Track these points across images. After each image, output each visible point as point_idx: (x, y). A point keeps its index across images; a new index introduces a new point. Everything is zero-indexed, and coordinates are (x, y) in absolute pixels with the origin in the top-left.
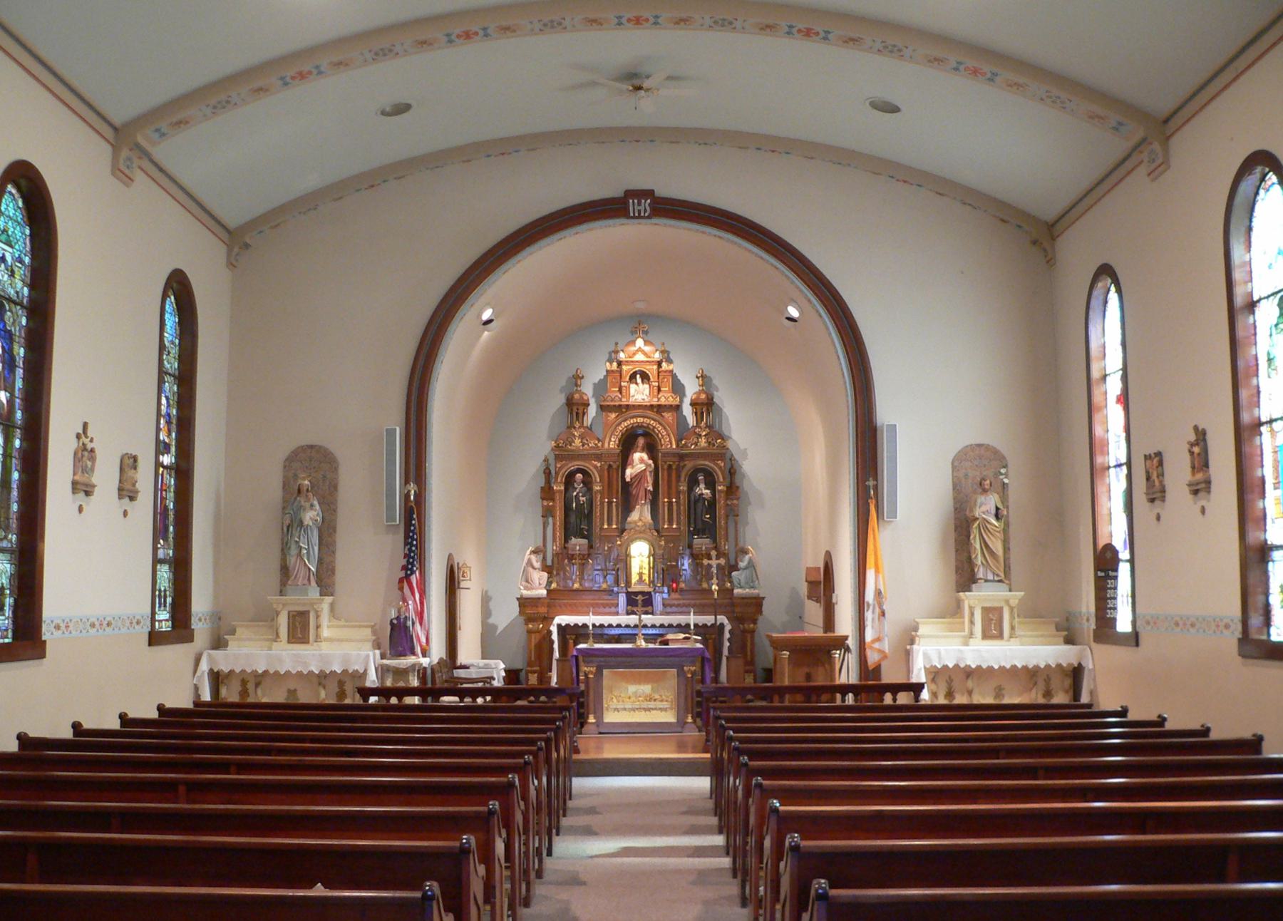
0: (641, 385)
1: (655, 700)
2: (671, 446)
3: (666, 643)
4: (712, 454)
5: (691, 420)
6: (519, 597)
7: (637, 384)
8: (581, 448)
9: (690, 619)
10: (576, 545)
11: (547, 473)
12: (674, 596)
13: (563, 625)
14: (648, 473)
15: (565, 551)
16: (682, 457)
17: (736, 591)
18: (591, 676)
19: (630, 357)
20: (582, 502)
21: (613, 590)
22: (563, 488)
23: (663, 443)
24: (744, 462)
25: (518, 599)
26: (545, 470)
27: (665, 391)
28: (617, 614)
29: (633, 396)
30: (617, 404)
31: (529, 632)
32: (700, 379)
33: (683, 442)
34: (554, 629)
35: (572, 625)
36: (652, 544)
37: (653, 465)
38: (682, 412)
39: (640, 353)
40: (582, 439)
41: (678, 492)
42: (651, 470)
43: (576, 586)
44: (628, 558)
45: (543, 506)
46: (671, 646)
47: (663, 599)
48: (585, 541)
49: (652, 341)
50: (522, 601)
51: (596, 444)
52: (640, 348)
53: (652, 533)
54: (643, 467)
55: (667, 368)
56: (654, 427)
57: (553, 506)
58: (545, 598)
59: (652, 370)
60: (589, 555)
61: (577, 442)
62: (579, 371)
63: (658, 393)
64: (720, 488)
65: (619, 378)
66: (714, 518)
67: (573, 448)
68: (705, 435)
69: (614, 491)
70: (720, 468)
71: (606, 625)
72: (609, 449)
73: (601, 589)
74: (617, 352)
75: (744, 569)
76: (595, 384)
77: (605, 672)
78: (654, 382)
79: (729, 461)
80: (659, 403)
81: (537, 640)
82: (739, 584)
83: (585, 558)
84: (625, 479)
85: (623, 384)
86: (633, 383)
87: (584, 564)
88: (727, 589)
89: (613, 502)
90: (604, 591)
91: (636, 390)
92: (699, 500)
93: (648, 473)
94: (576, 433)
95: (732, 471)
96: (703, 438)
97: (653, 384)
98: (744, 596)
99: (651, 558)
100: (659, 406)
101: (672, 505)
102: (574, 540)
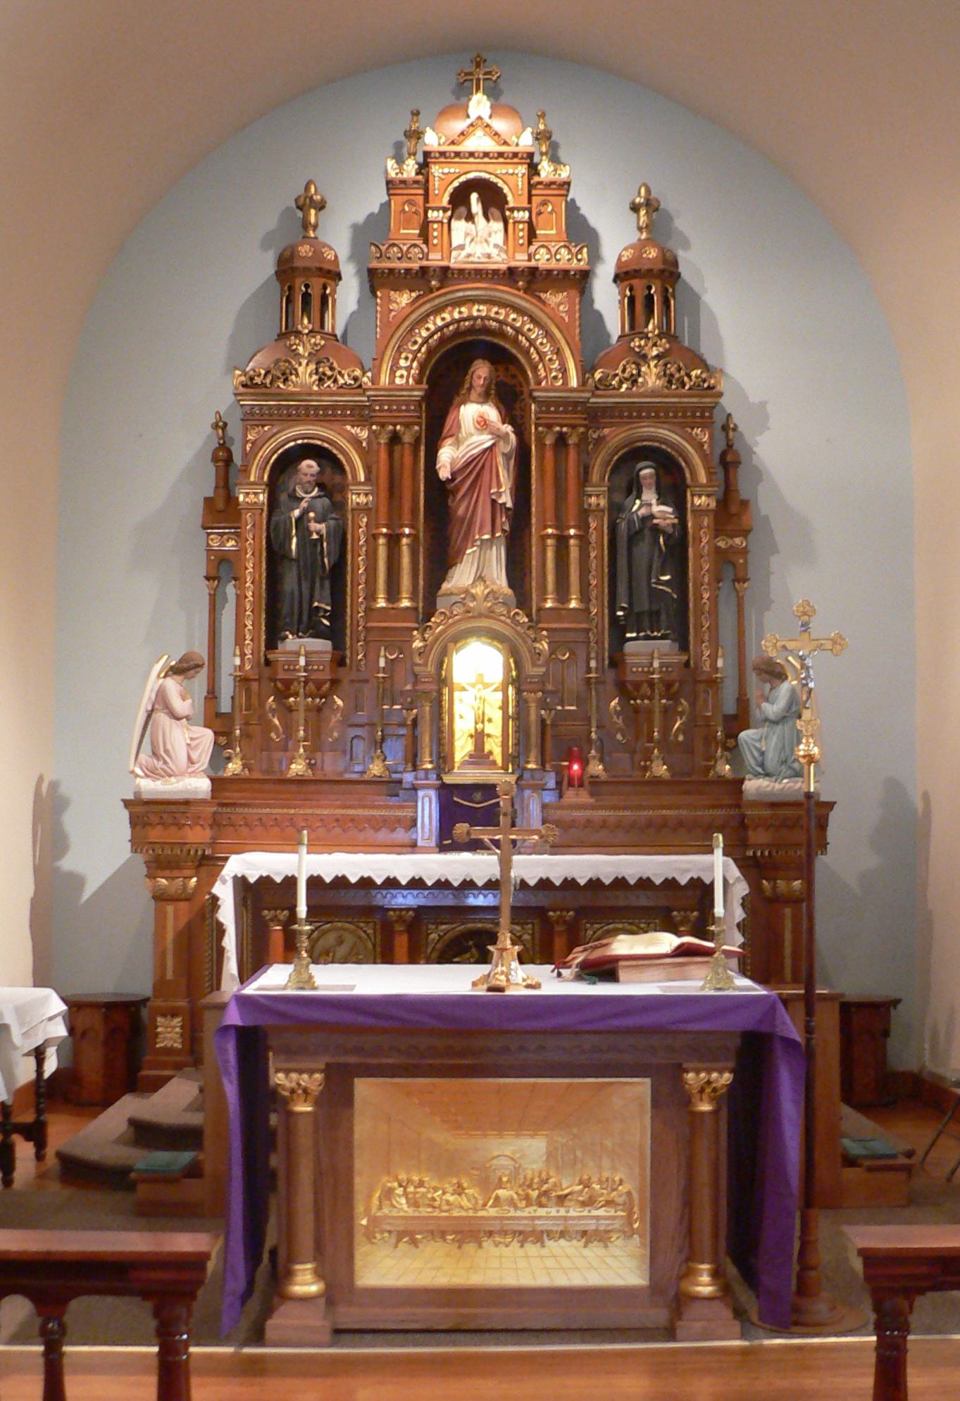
0: (480, 219)
1: (562, 1200)
2: (566, 382)
3: (606, 970)
4: (675, 408)
5: (614, 322)
6: (130, 797)
7: (470, 217)
8: (315, 388)
9: (711, 868)
10: (298, 654)
11: (223, 459)
12: (571, 796)
13: (252, 880)
14: (500, 460)
15: (267, 672)
16: (596, 416)
17: (753, 786)
18: (304, 1108)
19: (453, 143)
20: (315, 536)
21: (400, 782)
22: (262, 498)
23: (542, 373)
24: (758, 438)
25: (127, 803)
26: (215, 452)
27: (548, 239)
28: (413, 847)
29: (461, 247)
30: (415, 266)
31: (161, 898)
32: (643, 212)
33: (598, 375)
34: (224, 891)
35: (278, 880)
36: (513, 652)
37: (513, 437)
38: (592, 301)
39: (479, 132)
40: (318, 363)
41: (584, 514)
42: (507, 450)
43: (298, 768)
44: (446, 691)
45: (209, 551)
46: (629, 987)
47: (544, 807)
48: (323, 645)
49: (519, 110)
50: (139, 809)
51: (356, 379)
52: (480, 118)
53: (513, 618)
54: (486, 440)
55: (552, 177)
56: (518, 331)
57: (240, 553)
58: (203, 802)
59: (512, 180)
60: (335, 682)
61: (305, 374)
62: (313, 190)
63: (530, 243)
64: (697, 501)
65: (420, 200)
66: (681, 582)
67: (291, 388)
68: (658, 357)
69: (407, 505)
70: (699, 446)
71: (379, 881)
72: (393, 387)
73: (366, 777)
74: (417, 135)
75: (776, 723)
76: (355, 227)
77: (364, 1088)
78: (519, 209)
79: (723, 435)
80: (533, 263)
81: (183, 921)
82: (762, 765)
83: (323, 689)
84: (436, 473)
85: (432, 215)
86: (459, 218)
87: (319, 709)
88: (721, 781)
89: (403, 535)
90: (376, 782)
91: (467, 234)
92: (641, 530)
93: (500, 460)
94: (301, 349)
95: (729, 458)
96: (652, 364)
97: (517, 214)
98: (774, 799)
99: (511, 691)
100: (533, 271)
101: (567, 547)
102: (291, 642)
